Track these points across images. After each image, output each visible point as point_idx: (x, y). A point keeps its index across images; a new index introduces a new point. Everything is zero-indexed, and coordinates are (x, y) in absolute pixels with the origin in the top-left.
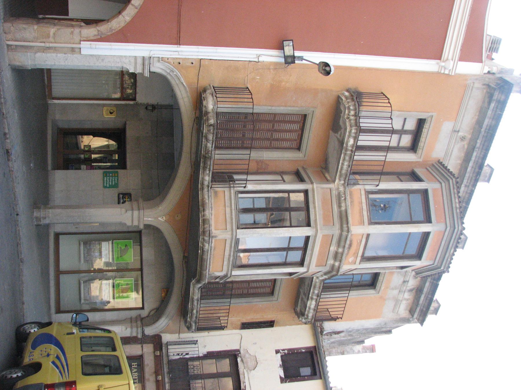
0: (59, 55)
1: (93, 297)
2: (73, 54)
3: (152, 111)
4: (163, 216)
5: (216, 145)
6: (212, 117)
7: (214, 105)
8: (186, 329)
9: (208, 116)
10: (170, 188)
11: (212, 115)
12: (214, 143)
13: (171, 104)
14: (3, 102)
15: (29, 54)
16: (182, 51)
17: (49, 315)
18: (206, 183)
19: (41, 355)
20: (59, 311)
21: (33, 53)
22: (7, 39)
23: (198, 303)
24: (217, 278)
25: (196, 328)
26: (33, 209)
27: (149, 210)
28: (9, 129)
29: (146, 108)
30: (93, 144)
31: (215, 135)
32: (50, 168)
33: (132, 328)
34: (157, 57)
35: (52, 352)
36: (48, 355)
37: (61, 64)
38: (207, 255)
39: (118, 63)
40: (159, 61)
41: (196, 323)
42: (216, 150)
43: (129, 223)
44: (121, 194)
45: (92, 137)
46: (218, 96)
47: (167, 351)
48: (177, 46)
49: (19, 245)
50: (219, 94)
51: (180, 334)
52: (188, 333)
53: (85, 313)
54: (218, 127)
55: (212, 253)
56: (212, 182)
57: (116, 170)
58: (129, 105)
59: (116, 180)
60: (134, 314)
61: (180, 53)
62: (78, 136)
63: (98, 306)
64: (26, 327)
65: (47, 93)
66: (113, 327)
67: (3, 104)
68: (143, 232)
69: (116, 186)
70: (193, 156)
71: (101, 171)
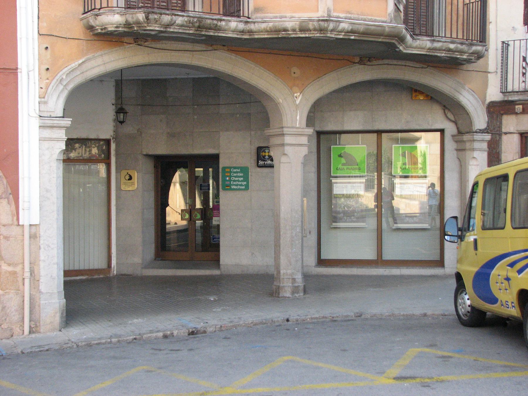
0: (42, 258)
1: (421, 208)
2: (40, 237)
3: (125, 113)
4: (293, 96)
5: (180, 9)
6: (134, 15)
7: (113, 12)
8: (481, 61)
9: (132, 23)
10: (245, 83)
11: (131, 16)
12: (177, 13)
13: (113, 83)
14: (116, 339)
15: (42, 302)
16: (28, 66)
17: (446, 277)
18: (241, 26)
19: (506, 289)
20: (440, 263)
21: (41, 296)
22: (21, 334)
23: (439, 41)
24: (397, 9)
25: (480, 44)
26: (279, 297)
27: (284, 119)
28: (158, 331)
29: (122, 122)
30: (180, 206)
31: (163, 11)
32: (216, 272)
33: (473, 150)
34: (39, 106)
35: (504, 273)
36: (508, 279)
37: (56, 255)
38: (360, 24)
39: (51, 167)
40: (46, 103)
41: (472, 45)
42: (187, 9)
43: (304, 151)
44: (258, 162)
45: (168, 209)
46: (98, 6)
47: (517, 92)
48: (19, 74)
49: (335, 319)
50: (95, 5)
51: (489, 71)
52: (488, 57)
53: (445, 220)
54: (149, 5)
55: (356, 16)
56: (239, 16)
57: (220, 170)
58: (117, 151)
59: (235, 170)
60: (450, 145)
61: (31, 68)
62: (167, 231)
63: (435, 202)
64: (461, 311)
65: (101, 276)
66: (470, 179)
67: (120, 339)
68: (318, 129)
69: (245, 171)
70: (198, 47)
71: (222, 194)
